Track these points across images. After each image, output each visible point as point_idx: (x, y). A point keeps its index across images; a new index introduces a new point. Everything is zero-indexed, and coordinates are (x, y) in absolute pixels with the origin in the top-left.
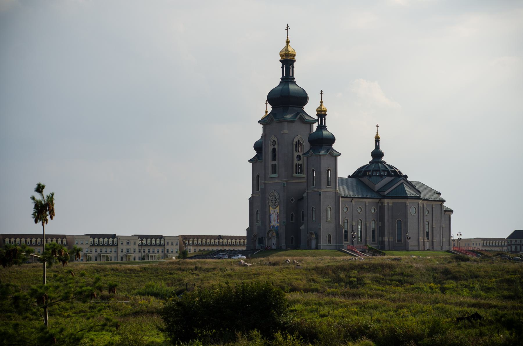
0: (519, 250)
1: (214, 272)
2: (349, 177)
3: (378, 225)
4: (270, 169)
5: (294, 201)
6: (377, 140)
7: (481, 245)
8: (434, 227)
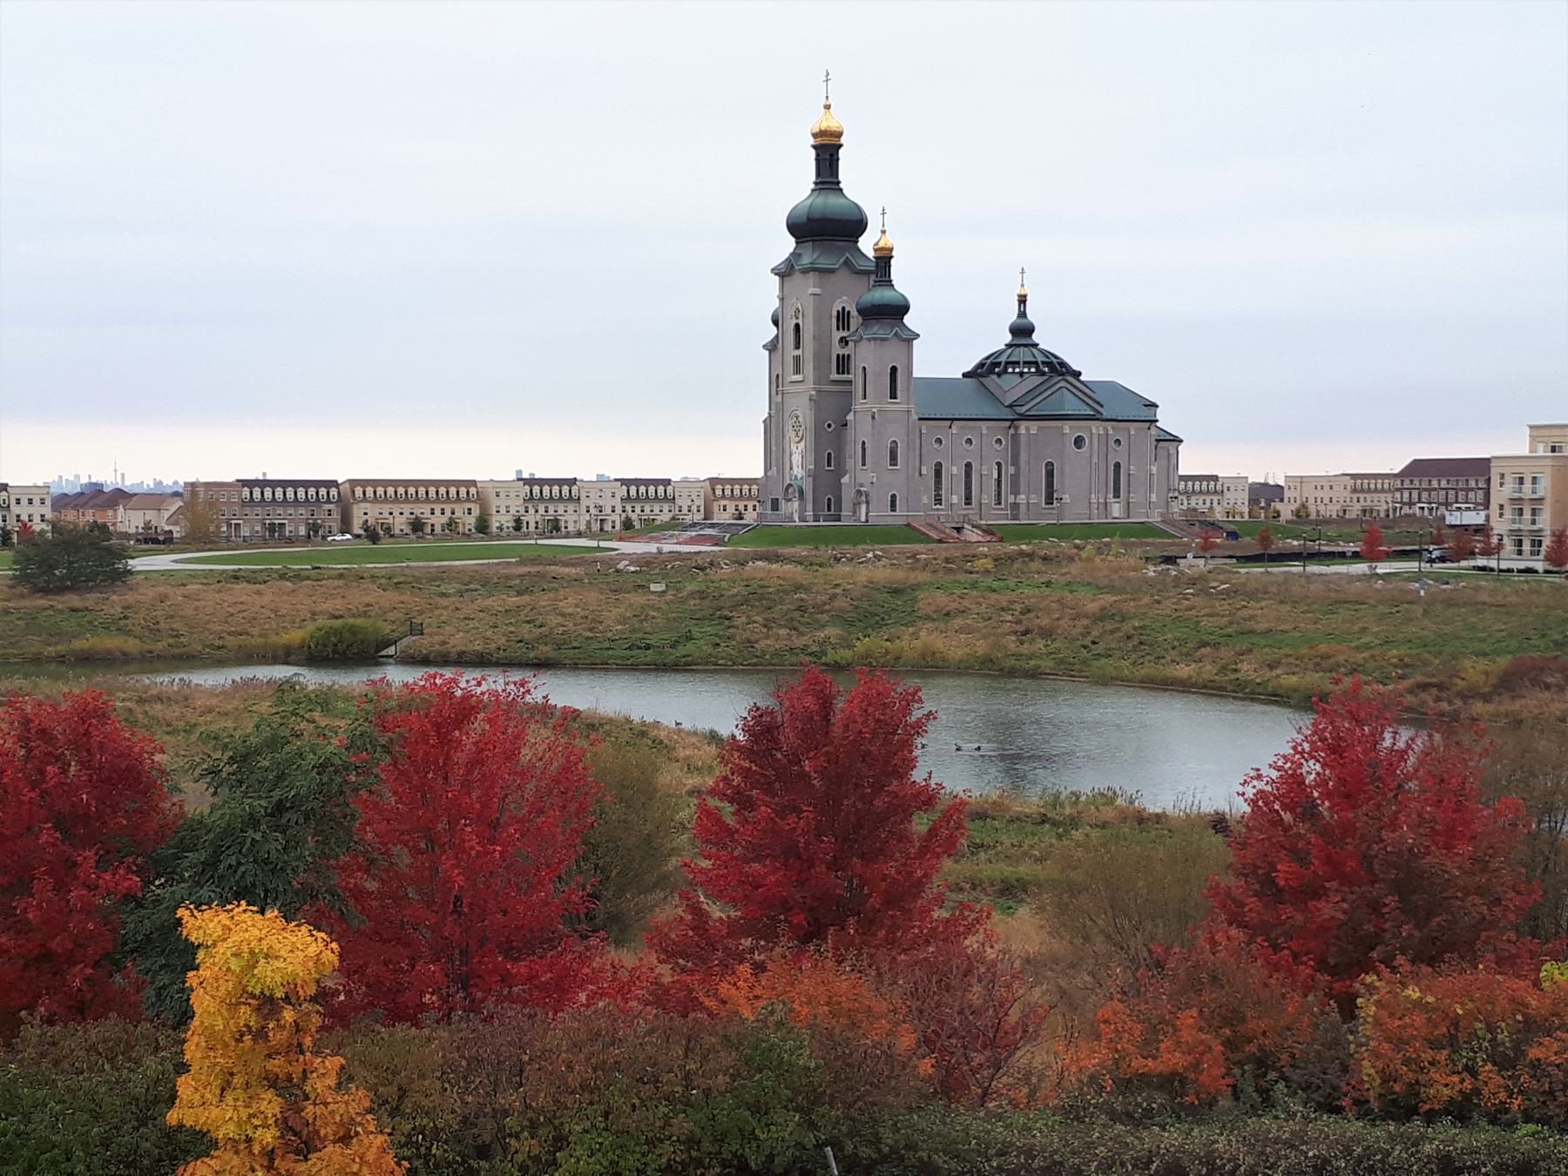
0: (1416, 500)
1: (489, 602)
2: (965, 375)
6: (1022, 300)
7: (1349, 487)
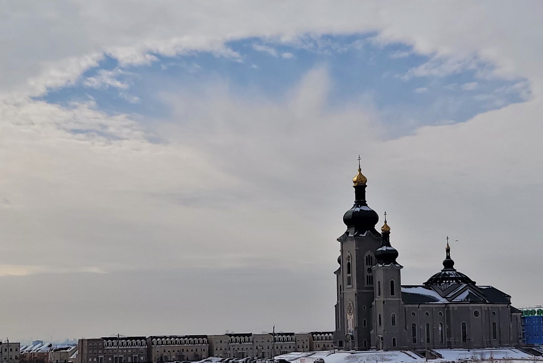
3: (445, 328)
4: (346, 282)
5: (363, 306)
8: (500, 327)
